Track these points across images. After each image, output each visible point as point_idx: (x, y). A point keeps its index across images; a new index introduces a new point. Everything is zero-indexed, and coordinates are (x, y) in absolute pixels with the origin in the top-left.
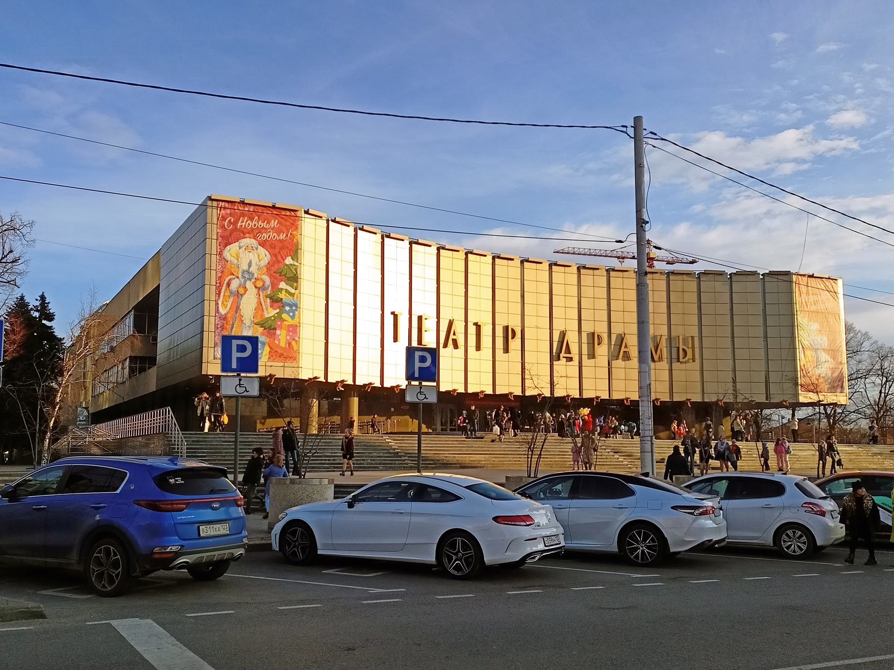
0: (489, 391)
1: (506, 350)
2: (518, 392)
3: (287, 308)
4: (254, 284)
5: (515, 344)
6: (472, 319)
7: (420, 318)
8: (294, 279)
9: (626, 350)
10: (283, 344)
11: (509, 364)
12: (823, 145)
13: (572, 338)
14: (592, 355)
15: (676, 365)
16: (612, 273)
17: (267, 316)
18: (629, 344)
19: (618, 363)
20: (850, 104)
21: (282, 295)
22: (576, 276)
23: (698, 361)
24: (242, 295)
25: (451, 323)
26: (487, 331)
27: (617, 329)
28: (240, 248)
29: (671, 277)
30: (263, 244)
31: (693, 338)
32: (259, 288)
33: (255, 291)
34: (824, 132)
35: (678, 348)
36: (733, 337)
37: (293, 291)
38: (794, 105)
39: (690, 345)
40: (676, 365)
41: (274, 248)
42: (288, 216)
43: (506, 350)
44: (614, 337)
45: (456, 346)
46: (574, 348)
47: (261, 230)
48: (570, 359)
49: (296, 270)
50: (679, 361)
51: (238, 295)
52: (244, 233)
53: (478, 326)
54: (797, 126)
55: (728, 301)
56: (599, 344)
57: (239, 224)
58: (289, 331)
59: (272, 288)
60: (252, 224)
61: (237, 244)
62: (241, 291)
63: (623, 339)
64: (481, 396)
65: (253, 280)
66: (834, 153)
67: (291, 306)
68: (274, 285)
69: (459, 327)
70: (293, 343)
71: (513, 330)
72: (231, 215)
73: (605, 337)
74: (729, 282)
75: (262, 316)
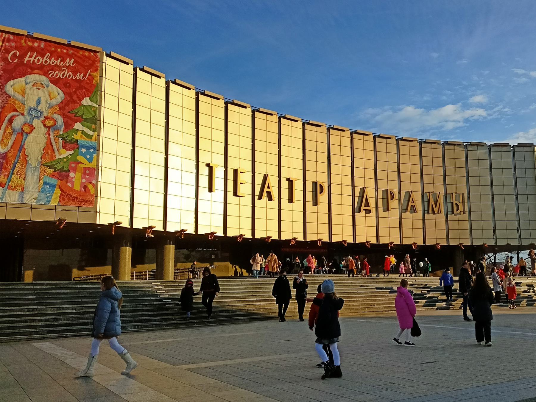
0: (301, 238)
1: (315, 203)
2: (326, 239)
3: (84, 150)
4: (43, 122)
5: (323, 198)
6: (285, 174)
7: (235, 171)
8: (95, 122)
9: (413, 204)
10: (77, 187)
11: (318, 215)
12: (468, 113)
13: (370, 193)
14: (386, 209)
15: (450, 216)
16: (401, 143)
17: (58, 157)
18: (415, 199)
19: (407, 215)
20: (479, 92)
21: (77, 136)
22: (372, 143)
23: (467, 213)
24: (27, 134)
25: (265, 177)
26: (298, 186)
27: (405, 187)
28: (26, 84)
29: (446, 147)
30: (55, 82)
31: (463, 195)
32: (49, 128)
33: (44, 130)
34: (466, 106)
35: (452, 203)
36: (492, 194)
37: (91, 133)
38: (449, 92)
39: (461, 201)
40: (450, 216)
41: (69, 87)
42: (89, 62)
43: (315, 203)
44: (403, 194)
45: (270, 198)
46: (372, 202)
47: (55, 68)
48: (369, 212)
49: (95, 112)
50: (453, 213)
51: (22, 134)
52: (32, 68)
53: (290, 182)
54: (453, 104)
55: (488, 166)
56: (392, 199)
57: (27, 59)
58: (85, 173)
59: (66, 128)
60: (42, 60)
61: (23, 79)
62: (27, 129)
63: (410, 196)
64: (292, 243)
65: (42, 119)
66: (474, 118)
67: (88, 148)
68: (68, 126)
69: (273, 181)
70: (90, 187)
71: (321, 186)
72: (16, 48)
73: (396, 193)
74: (488, 152)
75: (52, 157)
